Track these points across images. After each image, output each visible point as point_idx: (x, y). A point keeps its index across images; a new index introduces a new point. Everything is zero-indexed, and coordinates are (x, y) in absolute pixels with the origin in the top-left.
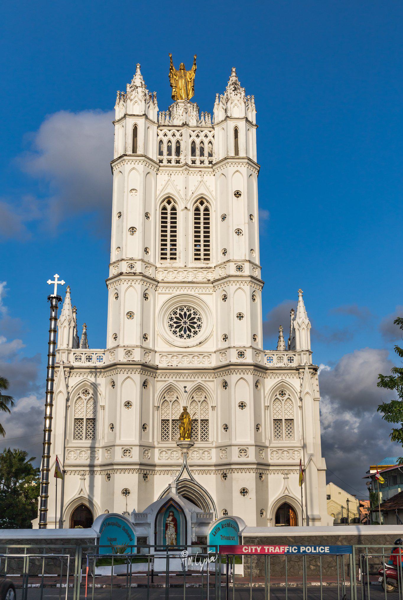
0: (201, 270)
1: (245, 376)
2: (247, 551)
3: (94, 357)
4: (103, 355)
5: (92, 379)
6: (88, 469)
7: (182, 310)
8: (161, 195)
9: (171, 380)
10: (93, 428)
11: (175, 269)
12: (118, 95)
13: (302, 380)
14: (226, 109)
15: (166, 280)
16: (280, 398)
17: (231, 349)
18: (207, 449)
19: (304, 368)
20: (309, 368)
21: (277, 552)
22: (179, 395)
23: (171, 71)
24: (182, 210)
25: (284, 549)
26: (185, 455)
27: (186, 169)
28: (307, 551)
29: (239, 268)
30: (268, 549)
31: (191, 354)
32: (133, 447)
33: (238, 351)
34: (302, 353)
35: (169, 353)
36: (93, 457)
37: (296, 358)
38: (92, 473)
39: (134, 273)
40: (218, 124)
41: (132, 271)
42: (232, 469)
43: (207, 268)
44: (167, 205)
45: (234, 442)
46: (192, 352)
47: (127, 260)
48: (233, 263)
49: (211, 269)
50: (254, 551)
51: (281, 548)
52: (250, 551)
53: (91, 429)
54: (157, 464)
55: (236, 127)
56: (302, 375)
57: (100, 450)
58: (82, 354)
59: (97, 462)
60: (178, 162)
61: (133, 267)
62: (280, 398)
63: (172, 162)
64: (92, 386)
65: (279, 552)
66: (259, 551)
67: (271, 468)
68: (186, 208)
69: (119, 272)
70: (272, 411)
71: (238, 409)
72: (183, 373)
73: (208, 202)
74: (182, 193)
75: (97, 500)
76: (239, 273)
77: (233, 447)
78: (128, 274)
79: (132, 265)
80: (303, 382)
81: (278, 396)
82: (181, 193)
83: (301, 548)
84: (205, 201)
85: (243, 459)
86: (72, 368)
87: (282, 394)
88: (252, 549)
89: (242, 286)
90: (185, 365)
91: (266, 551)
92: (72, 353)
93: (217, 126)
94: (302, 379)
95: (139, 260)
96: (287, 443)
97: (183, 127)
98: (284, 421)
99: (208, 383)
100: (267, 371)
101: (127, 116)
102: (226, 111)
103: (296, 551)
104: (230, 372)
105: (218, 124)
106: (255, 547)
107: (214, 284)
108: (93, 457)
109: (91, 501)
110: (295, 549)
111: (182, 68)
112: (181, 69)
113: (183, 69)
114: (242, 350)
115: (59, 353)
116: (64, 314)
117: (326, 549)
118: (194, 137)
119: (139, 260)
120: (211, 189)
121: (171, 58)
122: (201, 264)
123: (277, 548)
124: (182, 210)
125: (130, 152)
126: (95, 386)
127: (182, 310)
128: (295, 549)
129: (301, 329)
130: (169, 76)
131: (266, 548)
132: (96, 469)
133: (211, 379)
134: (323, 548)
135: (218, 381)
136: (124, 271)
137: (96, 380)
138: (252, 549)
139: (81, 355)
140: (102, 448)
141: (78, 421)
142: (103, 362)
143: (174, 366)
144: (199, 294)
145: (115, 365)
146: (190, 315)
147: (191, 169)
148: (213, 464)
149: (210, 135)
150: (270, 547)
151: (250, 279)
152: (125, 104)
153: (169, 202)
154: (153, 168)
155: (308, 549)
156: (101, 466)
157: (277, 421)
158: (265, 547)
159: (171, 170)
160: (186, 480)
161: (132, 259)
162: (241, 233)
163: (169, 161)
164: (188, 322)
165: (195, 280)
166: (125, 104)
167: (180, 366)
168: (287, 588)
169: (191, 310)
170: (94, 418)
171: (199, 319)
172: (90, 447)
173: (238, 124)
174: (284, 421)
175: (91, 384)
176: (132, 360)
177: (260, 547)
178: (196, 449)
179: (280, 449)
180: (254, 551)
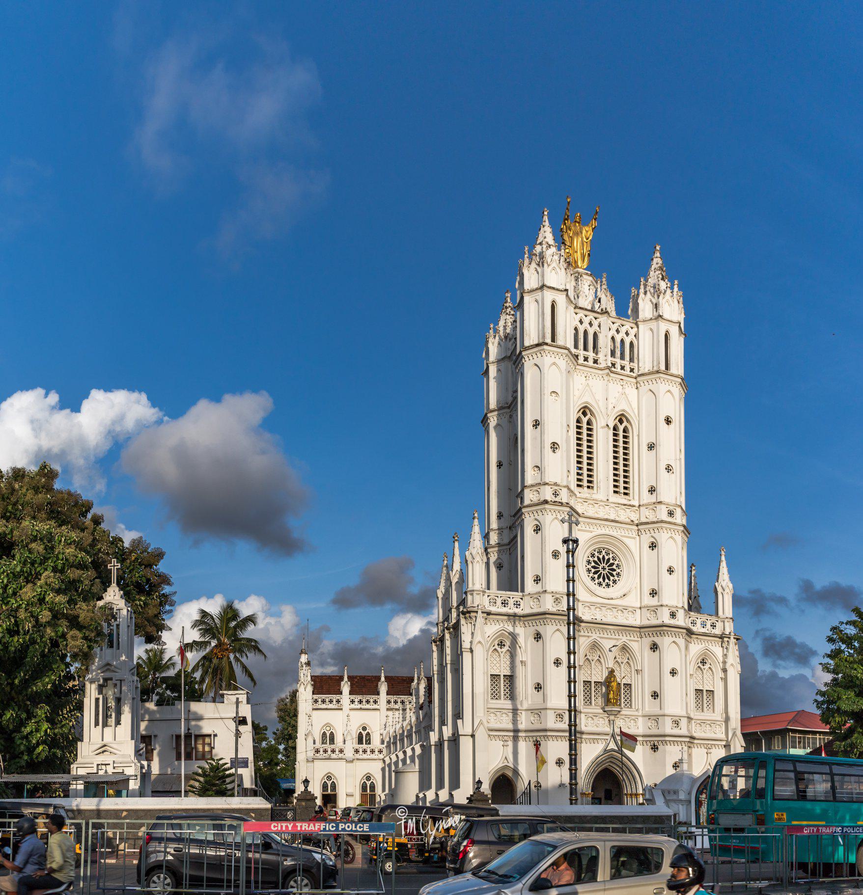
0: (623, 507)
1: (677, 640)
2: (276, 828)
3: (511, 602)
4: (521, 600)
5: (510, 629)
6: (511, 734)
7: (600, 552)
8: (579, 404)
9: (595, 636)
10: (509, 686)
11: (596, 502)
12: (527, 252)
13: (725, 650)
14: (656, 304)
15: (586, 514)
16: (499, 649)
17: (663, 608)
18: (633, 717)
19: (477, 612)
20: (482, 612)
21: (312, 830)
22: (602, 653)
23: (566, 221)
24: (602, 427)
25: (320, 826)
26: (611, 723)
27: (608, 375)
28: (347, 829)
29: (671, 514)
30: (301, 827)
31: (615, 607)
32: (682, 719)
33: (670, 611)
34: (726, 620)
35: (593, 604)
36: (515, 721)
37: (719, 625)
38: (516, 739)
39: (560, 502)
40: (644, 321)
41: (557, 499)
42: (666, 741)
43: (630, 505)
44: (582, 417)
45: (667, 712)
46: (616, 605)
47: (551, 485)
48: (665, 506)
49: (634, 508)
50: (284, 829)
51: (317, 825)
52: (279, 829)
53: (507, 688)
54: (586, 731)
55: (554, 301)
56: (474, 619)
57: (523, 713)
58: (510, 598)
59: (521, 727)
60: (595, 362)
61: (558, 495)
62: (499, 649)
63: (589, 360)
64: (510, 637)
65: (314, 829)
66: (290, 829)
67: (696, 741)
68: (607, 425)
69: (542, 499)
70: (489, 664)
71: (670, 676)
72: (608, 629)
73: (628, 421)
74: (601, 404)
75: (523, 769)
76: (670, 519)
77: (666, 717)
78: (555, 503)
79: (556, 492)
80: (474, 630)
81: (496, 647)
82: (600, 404)
83: (340, 825)
84: (624, 419)
85: (676, 731)
86: (489, 614)
87: (501, 645)
88: (282, 827)
89: (673, 535)
90: (609, 619)
91: (299, 829)
92: (486, 595)
93: (642, 323)
94: (727, 648)
95: (565, 487)
96: (707, 716)
97: (603, 316)
98: (502, 677)
99: (633, 643)
100: (692, 636)
101: (545, 288)
102: (656, 306)
103: (334, 828)
104: (662, 634)
105: (644, 321)
106: (286, 824)
107: (640, 527)
108: (515, 721)
109: (516, 772)
110: (333, 827)
111: (578, 220)
112: (576, 221)
113: (579, 223)
114: (674, 610)
115: (472, 594)
116: (475, 546)
117: (365, 827)
118: (613, 332)
119: (565, 487)
120: (633, 407)
121: (569, 203)
122: (621, 499)
123: (312, 825)
124: (602, 427)
125: (548, 340)
126: (514, 637)
127: (600, 552)
128: (333, 827)
129: (475, 561)
130: (561, 229)
131: (299, 825)
132: (520, 734)
133: (636, 639)
134: (362, 826)
135: (647, 642)
136: (549, 499)
137: (514, 630)
138: (282, 827)
139: (496, 598)
140: (526, 710)
141: (495, 677)
142: (521, 609)
143: (599, 621)
144: (622, 536)
145: (544, 614)
146: (609, 560)
147: (612, 375)
148: (641, 734)
149: (632, 332)
150: (304, 824)
151: (682, 528)
152: (539, 270)
153: (585, 414)
154: (650, 383)
155: (348, 827)
156: (526, 731)
157: (699, 691)
158: (297, 824)
159: (590, 372)
160: (613, 750)
161: (556, 484)
162: (671, 470)
163: (586, 359)
164: (600, 569)
165: (617, 519)
166: (539, 270)
167: (605, 620)
168: (205, 878)
169: (609, 554)
170: (512, 674)
171: (618, 566)
172: (513, 710)
173: (555, 297)
174: (502, 677)
175: (509, 633)
176: (562, 609)
177: (292, 824)
178: (623, 717)
179: (703, 722)
180: (284, 829)
